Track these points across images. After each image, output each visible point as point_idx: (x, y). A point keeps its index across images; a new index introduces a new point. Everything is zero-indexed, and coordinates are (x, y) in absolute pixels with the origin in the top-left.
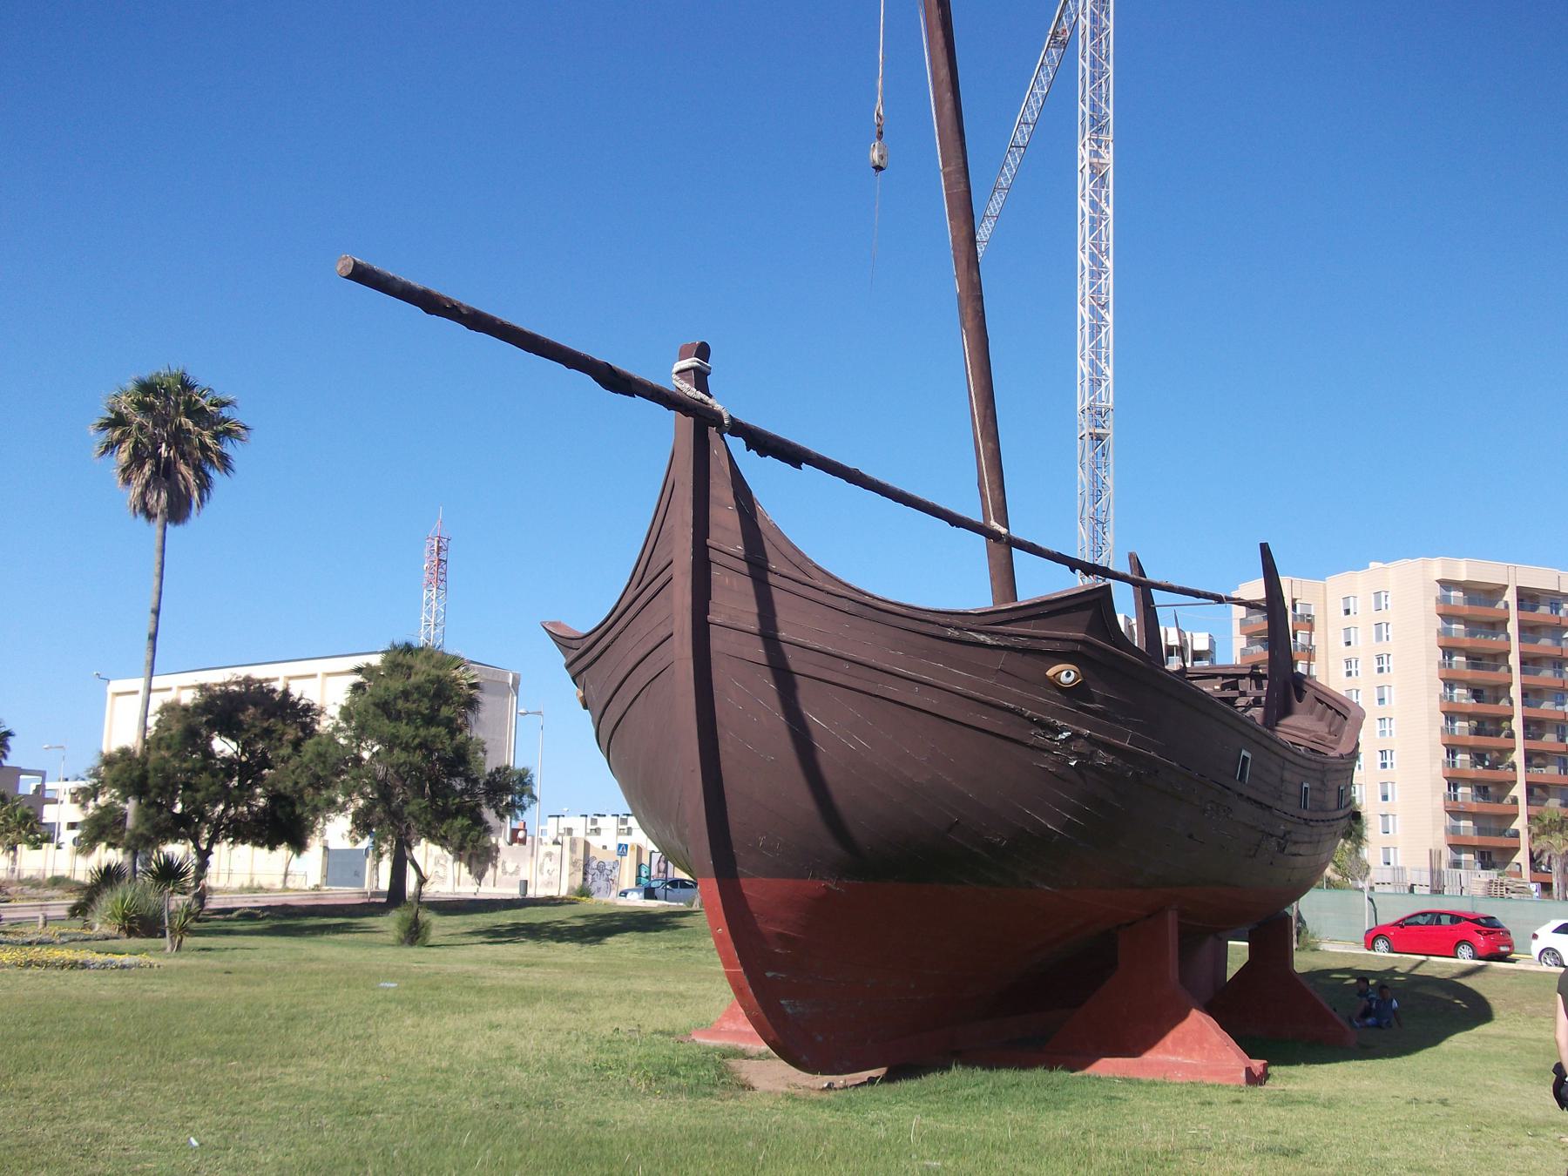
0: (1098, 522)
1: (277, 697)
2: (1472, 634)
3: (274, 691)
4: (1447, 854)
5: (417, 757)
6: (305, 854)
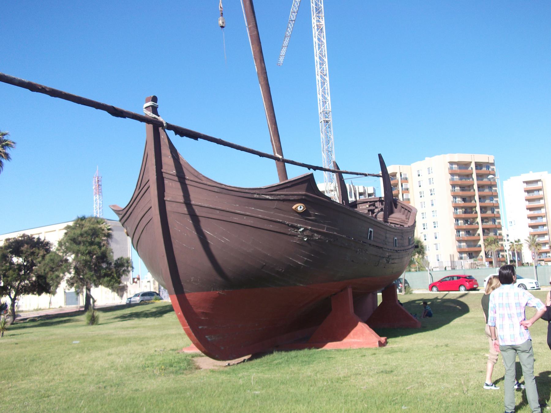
0: (329, 151)
1: (35, 240)
2: (461, 179)
3: (34, 238)
4: (457, 255)
5: (88, 258)
6: (56, 295)
